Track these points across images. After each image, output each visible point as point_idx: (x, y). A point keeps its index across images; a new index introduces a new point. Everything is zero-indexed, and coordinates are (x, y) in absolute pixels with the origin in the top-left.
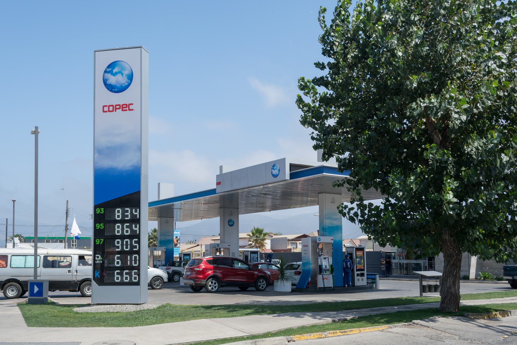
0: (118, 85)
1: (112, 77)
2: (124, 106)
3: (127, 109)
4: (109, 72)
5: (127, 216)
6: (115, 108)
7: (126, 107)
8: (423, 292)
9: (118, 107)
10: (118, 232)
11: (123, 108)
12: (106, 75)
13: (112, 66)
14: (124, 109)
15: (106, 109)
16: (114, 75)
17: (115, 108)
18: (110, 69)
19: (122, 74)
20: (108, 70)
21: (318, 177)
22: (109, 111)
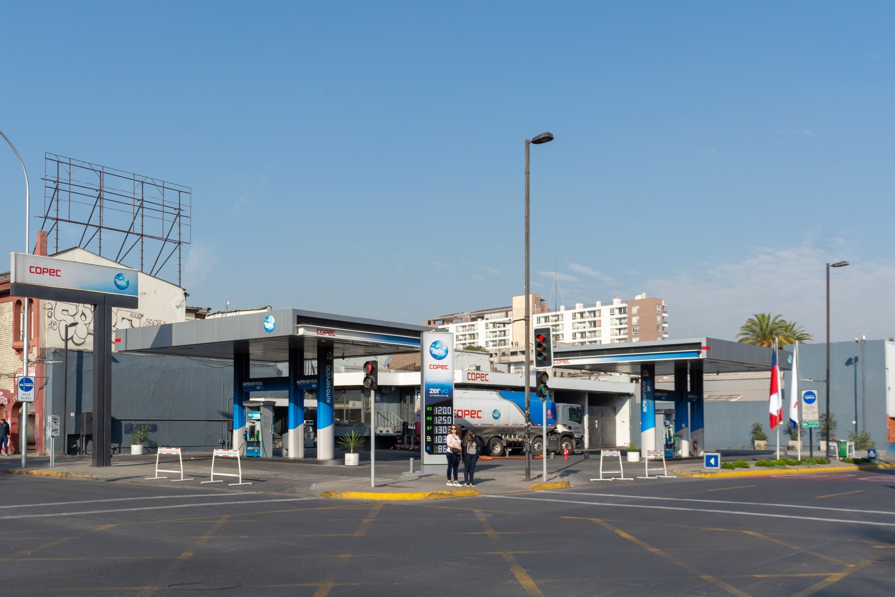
0: (439, 355)
1: (435, 350)
2: (472, 412)
3: (476, 416)
4: (433, 347)
5: (440, 431)
6: (437, 367)
7: (443, 367)
8: (316, 457)
9: (467, 413)
10: (440, 450)
11: (472, 414)
12: (432, 348)
13: (435, 343)
14: (473, 416)
15: (432, 367)
16: (437, 348)
17: (437, 367)
18: (434, 345)
19: (442, 349)
20: (433, 345)
21: (228, 469)
22: (434, 368)
